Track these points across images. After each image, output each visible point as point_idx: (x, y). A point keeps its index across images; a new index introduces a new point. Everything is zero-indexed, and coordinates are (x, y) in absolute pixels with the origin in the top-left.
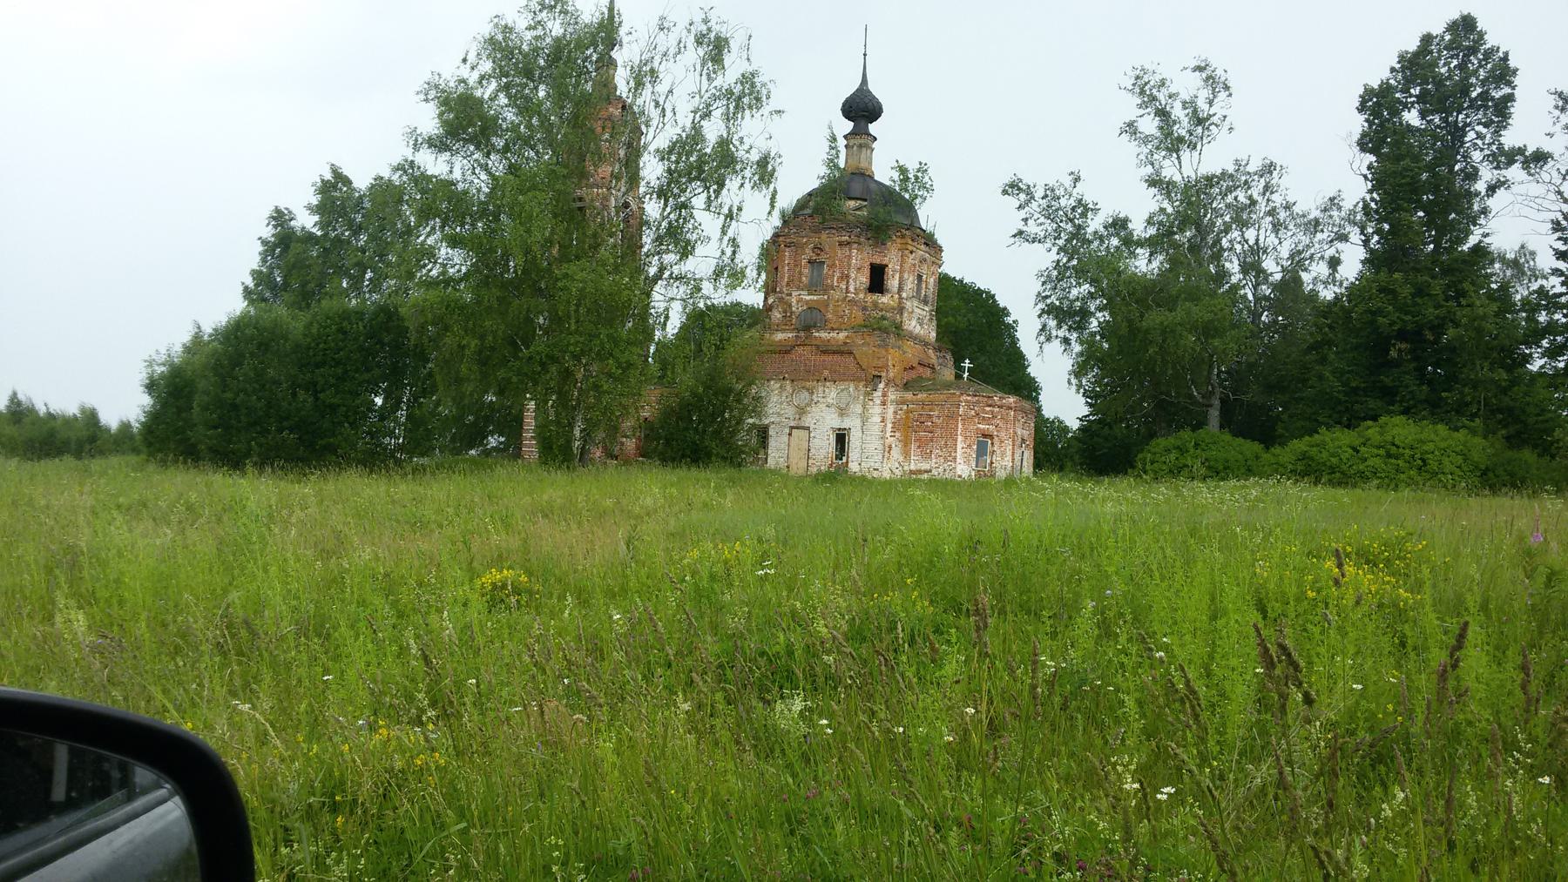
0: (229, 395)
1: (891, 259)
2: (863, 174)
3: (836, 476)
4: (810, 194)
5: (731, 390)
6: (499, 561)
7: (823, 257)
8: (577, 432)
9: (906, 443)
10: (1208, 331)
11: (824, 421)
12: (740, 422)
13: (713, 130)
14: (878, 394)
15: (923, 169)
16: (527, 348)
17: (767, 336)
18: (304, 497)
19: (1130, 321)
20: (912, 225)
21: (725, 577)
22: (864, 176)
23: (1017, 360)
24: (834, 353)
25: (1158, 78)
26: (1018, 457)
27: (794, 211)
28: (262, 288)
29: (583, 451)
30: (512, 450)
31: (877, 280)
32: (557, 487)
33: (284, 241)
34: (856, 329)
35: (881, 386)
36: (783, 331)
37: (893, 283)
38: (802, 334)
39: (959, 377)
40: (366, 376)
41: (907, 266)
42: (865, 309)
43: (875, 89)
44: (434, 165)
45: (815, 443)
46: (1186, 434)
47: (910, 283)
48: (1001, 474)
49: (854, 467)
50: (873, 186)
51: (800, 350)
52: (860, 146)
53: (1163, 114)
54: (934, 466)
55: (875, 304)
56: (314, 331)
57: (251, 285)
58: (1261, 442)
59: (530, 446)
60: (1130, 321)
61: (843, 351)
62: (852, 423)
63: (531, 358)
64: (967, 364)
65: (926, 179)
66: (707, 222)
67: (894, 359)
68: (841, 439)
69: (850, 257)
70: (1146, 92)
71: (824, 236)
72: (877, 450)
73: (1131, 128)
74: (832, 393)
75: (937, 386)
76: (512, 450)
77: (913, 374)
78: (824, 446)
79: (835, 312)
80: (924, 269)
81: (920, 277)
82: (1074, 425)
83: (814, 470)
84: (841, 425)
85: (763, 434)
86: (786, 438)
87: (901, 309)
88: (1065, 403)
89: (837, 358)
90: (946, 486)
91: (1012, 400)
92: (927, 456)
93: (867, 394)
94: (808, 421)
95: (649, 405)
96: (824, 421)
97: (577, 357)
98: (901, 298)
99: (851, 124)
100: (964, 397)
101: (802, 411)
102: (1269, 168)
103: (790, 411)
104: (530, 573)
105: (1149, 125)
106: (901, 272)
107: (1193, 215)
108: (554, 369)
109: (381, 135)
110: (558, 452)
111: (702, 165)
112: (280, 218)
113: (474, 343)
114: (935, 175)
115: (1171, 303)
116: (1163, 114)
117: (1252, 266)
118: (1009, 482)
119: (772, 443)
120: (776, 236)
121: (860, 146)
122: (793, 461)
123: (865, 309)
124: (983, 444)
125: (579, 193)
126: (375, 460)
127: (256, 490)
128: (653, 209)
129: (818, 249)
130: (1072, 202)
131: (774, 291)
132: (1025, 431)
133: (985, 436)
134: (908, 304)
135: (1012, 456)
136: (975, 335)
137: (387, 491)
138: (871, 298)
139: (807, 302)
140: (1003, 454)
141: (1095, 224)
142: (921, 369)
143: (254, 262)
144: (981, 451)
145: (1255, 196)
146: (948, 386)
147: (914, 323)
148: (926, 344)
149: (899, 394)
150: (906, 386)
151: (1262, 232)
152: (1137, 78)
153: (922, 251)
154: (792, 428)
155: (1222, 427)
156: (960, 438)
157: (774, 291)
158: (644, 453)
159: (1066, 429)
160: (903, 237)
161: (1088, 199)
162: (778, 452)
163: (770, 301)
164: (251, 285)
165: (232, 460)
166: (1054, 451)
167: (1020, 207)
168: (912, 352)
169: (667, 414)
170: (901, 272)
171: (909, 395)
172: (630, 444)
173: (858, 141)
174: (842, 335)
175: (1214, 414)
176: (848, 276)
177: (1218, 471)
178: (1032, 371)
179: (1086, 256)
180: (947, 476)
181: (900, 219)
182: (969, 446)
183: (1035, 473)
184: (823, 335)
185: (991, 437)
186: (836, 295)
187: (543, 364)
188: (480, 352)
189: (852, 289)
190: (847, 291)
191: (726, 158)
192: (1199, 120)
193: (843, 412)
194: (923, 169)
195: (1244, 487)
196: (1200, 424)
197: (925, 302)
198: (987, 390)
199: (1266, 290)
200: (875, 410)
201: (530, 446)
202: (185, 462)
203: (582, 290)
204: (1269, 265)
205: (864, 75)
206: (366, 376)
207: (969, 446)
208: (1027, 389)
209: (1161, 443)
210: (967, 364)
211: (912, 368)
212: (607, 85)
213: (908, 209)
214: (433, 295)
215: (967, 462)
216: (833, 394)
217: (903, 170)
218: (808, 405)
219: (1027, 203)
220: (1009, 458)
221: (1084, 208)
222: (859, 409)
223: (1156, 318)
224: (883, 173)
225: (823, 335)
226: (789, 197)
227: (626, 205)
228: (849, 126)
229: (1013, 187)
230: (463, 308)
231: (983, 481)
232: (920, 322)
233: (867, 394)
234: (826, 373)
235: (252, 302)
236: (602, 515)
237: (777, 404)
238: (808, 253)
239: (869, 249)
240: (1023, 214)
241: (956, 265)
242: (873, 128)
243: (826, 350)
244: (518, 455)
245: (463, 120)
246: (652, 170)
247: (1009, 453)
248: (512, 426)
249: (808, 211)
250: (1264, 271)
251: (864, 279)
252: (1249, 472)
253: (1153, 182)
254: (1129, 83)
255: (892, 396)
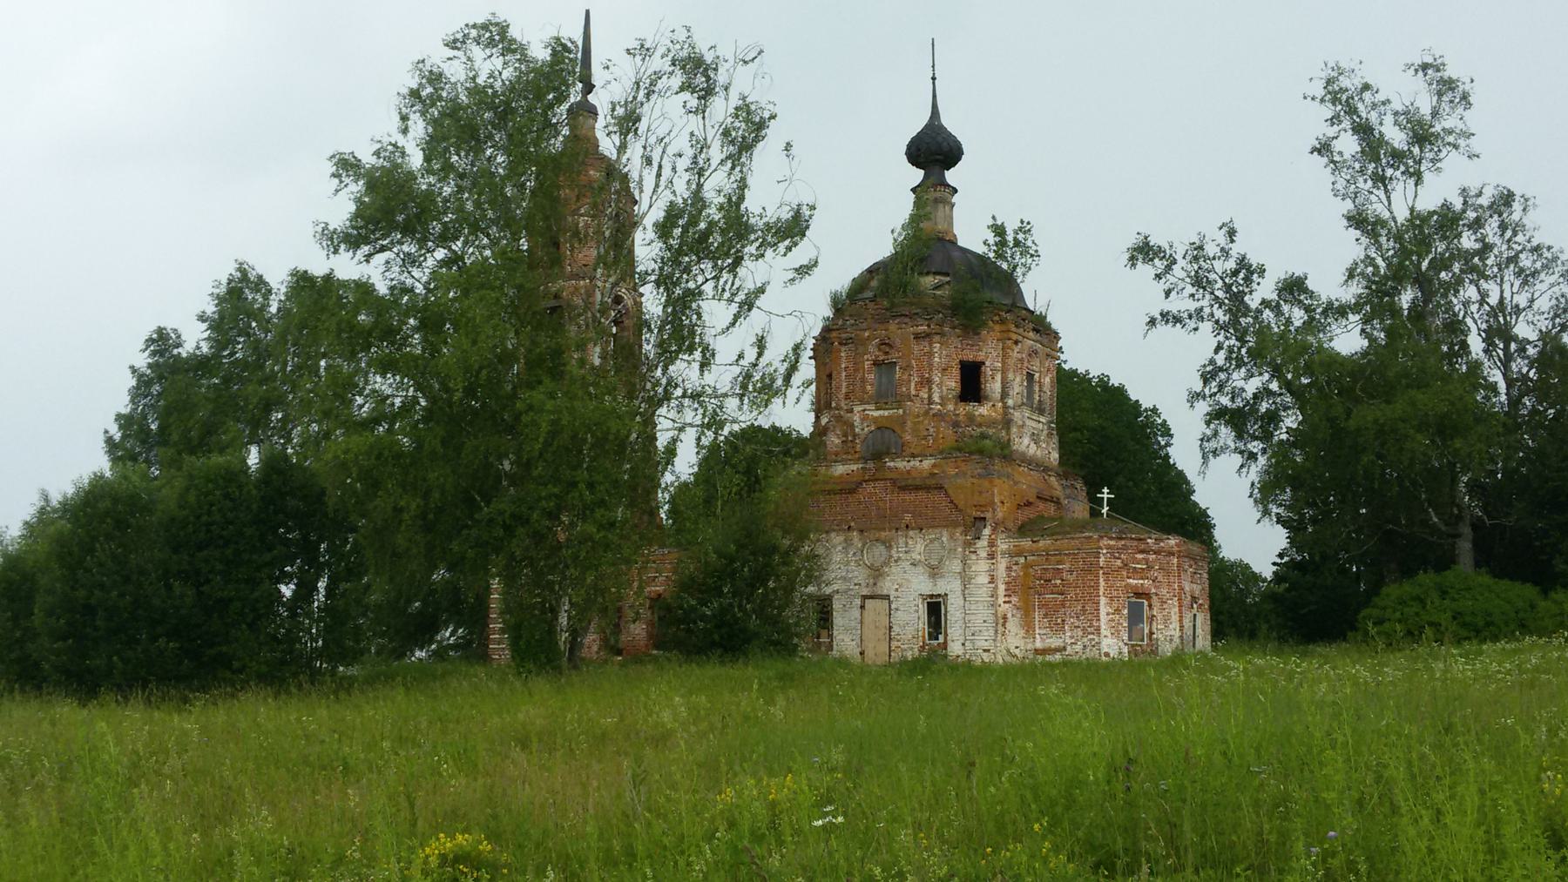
0: (82, 593)
1: (989, 353)
2: (941, 240)
3: (931, 660)
4: (872, 271)
5: (775, 549)
6: (453, 820)
7: (894, 356)
8: (563, 620)
9: (1026, 612)
10: (1445, 429)
11: (909, 585)
12: (790, 589)
13: (717, 183)
14: (983, 543)
15: (1024, 228)
16: (488, 504)
17: (823, 470)
18: (185, 733)
19: (1332, 421)
20: (1014, 305)
21: (772, 828)
22: (947, 241)
23: (1175, 486)
24: (917, 488)
25: (1358, 82)
26: (1187, 623)
27: (848, 295)
28: (133, 440)
29: (574, 645)
30: (474, 650)
31: (971, 383)
32: (536, 705)
33: (169, 378)
34: (944, 454)
35: (987, 531)
36: (844, 462)
37: (994, 387)
38: (870, 465)
39: (1095, 513)
40: (268, 557)
41: (1011, 362)
42: (956, 424)
43: (951, 122)
44: (347, 267)
45: (900, 617)
46: (1426, 578)
47: (1018, 386)
48: (1167, 649)
49: (955, 649)
50: (956, 254)
51: (869, 488)
52: (936, 201)
53: (1363, 130)
54: (1070, 642)
55: (971, 418)
56: (192, 498)
57: (117, 437)
58: (1536, 583)
59: (499, 646)
60: (1332, 421)
61: (930, 485)
62: (949, 586)
63: (491, 520)
64: (1105, 494)
65: (1029, 243)
66: (714, 313)
67: (1002, 496)
68: (935, 609)
69: (931, 354)
70: (1342, 99)
71: (893, 326)
72: (987, 626)
73: (1323, 148)
74: (918, 546)
75: (1065, 528)
76: (474, 650)
77: (1029, 513)
78: (910, 621)
79: (915, 431)
80: (1036, 365)
81: (1030, 376)
82: (1265, 567)
83: (895, 657)
84: (937, 594)
85: (824, 613)
86: (856, 613)
87: (1007, 423)
88: (1254, 540)
89: (922, 495)
90: (1092, 672)
91: (1172, 541)
92: (1058, 628)
93: (968, 544)
94: (887, 586)
95: (657, 575)
96: (909, 585)
97: (553, 516)
98: (1005, 407)
99: (922, 172)
100: (1105, 542)
101: (877, 573)
102: (1507, 199)
103: (860, 575)
104: (494, 836)
105: (1348, 145)
106: (1004, 372)
107: (1419, 263)
108: (521, 531)
109: (291, 230)
110: (539, 652)
111: (715, 237)
112: (162, 342)
113: (413, 504)
114: (1040, 238)
115: (1387, 392)
116: (1363, 130)
117: (1498, 333)
118: (1178, 659)
119: (838, 620)
120: (826, 330)
121: (936, 201)
122: (870, 653)
123: (956, 424)
124: (1137, 608)
125: (553, 287)
126: (285, 670)
127: (115, 731)
128: (653, 302)
129: (886, 345)
130: (1231, 264)
131: (828, 406)
132: (1195, 585)
133: (1138, 595)
134: (1017, 415)
135: (1179, 623)
136: (1110, 446)
137: (298, 720)
138: (964, 409)
139: (875, 420)
140: (1166, 620)
141: (1265, 289)
142: (1041, 505)
143: (123, 405)
144: (1135, 617)
145: (1490, 239)
146: (1081, 526)
147: (1026, 441)
148: (1046, 469)
149: (1014, 542)
150: (1023, 530)
151: (1506, 286)
152: (1329, 82)
153: (1030, 341)
154: (865, 597)
155: (1478, 564)
156: (1103, 601)
157: (828, 406)
158: (659, 641)
159: (1256, 577)
160: (1003, 321)
161: (1254, 260)
162: (845, 640)
163: (824, 421)
164: (117, 437)
165: (85, 683)
166: (1237, 608)
167: (1158, 277)
168: (1027, 482)
169: (687, 585)
170: (1004, 372)
171: (1026, 543)
172: (637, 631)
173: (932, 195)
174: (927, 463)
175: (1465, 547)
176: (929, 381)
177: (1477, 629)
178: (1201, 498)
179: (1261, 332)
180: (1089, 654)
181: (996, 296)
182: (1118, 611)
183: (1214, 648)
184: (901, 464)
185: (1147, 596)
186: (916, 407)
187: (507, 528)
188: (423, 516)
189: (936, 398)
190: (930, 401)
191: (737, 226)
192: (1422, 135)
193: (934, 572)
194: (1024, 228)
195: (1515, 651)
196: (1445, 562)
197: (1041, 411)
198: (1135, 529)
199: (1519, 366)
200: (980, 567)
201: (499, 646)
202: (23, 691)
203: (554, 423)
204: (1522, 330)
205: (934, 96)
206: (268, 557)
207: (1118, 611)
208: (1195, 526)
209: (1393, 591)
210: (1105, 494)
211: (1029, 504)
212: (583, 144)
213: (1008, 283)
214: (358, 441)
215: (1116, 633)
216: (920, 547)
217: (999, 230)
218: (886, 563)
219: (1168, 268)
220: (1175, 625)
221: (1247, 271)
222: (956, 566)
223: (1369, 414)
224: (971, 235)
225: (901, 464)
226: (839, 273)
227: (618, 300)
228: (918, 175)
229: (1144, 251)
230: (399, 455)
231: (1143, 654)
232: (1035, 438)
233: (968, 544)
234: (908, 517)
235: (115, 460)
236: (602, 738)
237: (841, 565)
238: (873, 351)
239: (956, 342)
240: (1162, 285)
241: (1080, 355)
242: (951, 176)
243: (906, 485)
244: (483, 656)
245: (388, 205)
246: (646, 250)
247: (1175, 617)
248: (476, 619)
249: (869, 294)
250: (1515, 338)
251: (953, 383)
252: (1525, 628)
253: (1358, 220)
254: (1319, 91)
255: (1003, 545)
